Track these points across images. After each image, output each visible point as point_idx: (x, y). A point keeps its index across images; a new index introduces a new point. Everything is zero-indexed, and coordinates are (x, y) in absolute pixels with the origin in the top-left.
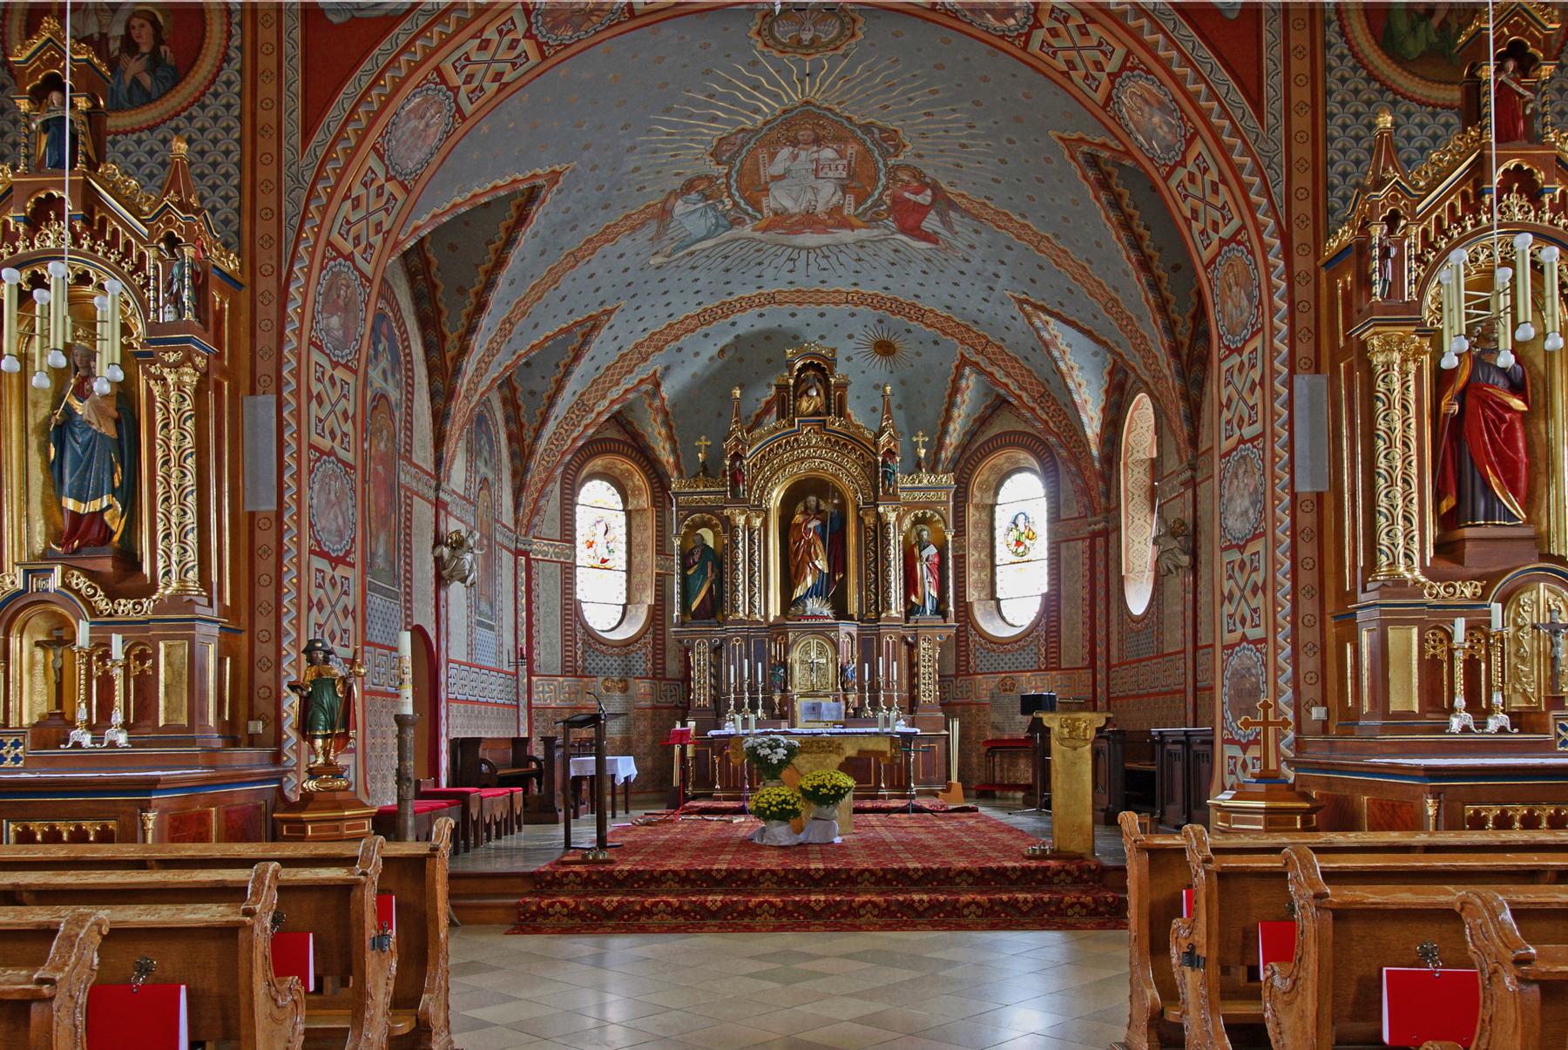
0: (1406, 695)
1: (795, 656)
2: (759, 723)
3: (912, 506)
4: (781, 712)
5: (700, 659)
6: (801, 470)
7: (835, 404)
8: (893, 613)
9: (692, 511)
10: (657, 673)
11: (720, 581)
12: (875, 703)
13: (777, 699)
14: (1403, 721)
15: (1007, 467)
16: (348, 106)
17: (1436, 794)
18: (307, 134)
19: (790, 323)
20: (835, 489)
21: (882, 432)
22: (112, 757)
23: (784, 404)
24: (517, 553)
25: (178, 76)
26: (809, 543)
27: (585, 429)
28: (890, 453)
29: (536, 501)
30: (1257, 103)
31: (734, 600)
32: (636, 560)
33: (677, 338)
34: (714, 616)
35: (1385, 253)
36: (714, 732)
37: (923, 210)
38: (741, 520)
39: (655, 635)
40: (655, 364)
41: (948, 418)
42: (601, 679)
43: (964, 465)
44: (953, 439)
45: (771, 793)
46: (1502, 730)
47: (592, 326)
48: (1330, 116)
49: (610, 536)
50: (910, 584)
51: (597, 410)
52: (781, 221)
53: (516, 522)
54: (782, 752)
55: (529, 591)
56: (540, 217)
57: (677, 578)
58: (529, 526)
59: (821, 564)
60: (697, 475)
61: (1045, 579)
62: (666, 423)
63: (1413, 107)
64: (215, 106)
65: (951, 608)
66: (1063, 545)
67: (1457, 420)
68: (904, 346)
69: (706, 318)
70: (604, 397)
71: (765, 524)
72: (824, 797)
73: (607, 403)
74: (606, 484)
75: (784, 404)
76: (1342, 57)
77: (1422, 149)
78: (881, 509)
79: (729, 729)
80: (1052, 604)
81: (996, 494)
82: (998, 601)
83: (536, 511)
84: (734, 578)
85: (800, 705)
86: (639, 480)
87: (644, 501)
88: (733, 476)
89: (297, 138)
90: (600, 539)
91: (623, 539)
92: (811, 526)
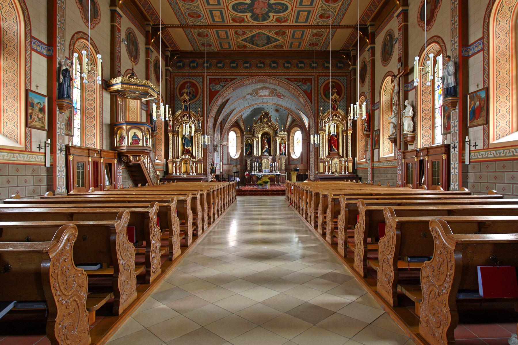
0: (322, 170)
1: (263, 162)
2: (258, 173)
3: (281, 137)
4: (260, 171)
5: (248, 162)
6: (263, 131)
7: (269, 120)
8: (278, 155)
10: (241, 164)
13: (260, 169)
14: (321, 173)
15: (296, 130)
18: (210, 104)
19: (262, 107)
20: (269, 134)
21: (276, 125)
22: (194, 176)
23: (261, 119)
24: (221, 144)
25: (196, 97)
26: (265, 143)
27: (230, 125)
28: (277, 129)
31: (254, 152)
35: (321, 123)
36: (251, 174)
37: (281, 96)
38: (255, 139)
40: (242, 113)
41: (287, 122)
43: (289, 131)
44: (288, 125)
45: (260, 182)
47: (233, 110)
48: (319, 104)
50: (280, 150)
52: (261, 96)
53: (221, 140)
54: (261, 176)
55: (222, 151)
56: (229, 101)
57: (245, 149)
58: (222, 140)
59: (267, 146)
62: (243, 122)
64: (199, 101)
67: (330, 140)
69: (249, 106)
71: (258, 140)
72: (266, 183)
75: (261, 119)
77: (327, 109)
79: (253, 173)
80: (302, 154)
83: (223, 138)
84: (254, 149)
85: (264, 169)
86: (238, 131)
87: (239, 135)
88: (254, 132)
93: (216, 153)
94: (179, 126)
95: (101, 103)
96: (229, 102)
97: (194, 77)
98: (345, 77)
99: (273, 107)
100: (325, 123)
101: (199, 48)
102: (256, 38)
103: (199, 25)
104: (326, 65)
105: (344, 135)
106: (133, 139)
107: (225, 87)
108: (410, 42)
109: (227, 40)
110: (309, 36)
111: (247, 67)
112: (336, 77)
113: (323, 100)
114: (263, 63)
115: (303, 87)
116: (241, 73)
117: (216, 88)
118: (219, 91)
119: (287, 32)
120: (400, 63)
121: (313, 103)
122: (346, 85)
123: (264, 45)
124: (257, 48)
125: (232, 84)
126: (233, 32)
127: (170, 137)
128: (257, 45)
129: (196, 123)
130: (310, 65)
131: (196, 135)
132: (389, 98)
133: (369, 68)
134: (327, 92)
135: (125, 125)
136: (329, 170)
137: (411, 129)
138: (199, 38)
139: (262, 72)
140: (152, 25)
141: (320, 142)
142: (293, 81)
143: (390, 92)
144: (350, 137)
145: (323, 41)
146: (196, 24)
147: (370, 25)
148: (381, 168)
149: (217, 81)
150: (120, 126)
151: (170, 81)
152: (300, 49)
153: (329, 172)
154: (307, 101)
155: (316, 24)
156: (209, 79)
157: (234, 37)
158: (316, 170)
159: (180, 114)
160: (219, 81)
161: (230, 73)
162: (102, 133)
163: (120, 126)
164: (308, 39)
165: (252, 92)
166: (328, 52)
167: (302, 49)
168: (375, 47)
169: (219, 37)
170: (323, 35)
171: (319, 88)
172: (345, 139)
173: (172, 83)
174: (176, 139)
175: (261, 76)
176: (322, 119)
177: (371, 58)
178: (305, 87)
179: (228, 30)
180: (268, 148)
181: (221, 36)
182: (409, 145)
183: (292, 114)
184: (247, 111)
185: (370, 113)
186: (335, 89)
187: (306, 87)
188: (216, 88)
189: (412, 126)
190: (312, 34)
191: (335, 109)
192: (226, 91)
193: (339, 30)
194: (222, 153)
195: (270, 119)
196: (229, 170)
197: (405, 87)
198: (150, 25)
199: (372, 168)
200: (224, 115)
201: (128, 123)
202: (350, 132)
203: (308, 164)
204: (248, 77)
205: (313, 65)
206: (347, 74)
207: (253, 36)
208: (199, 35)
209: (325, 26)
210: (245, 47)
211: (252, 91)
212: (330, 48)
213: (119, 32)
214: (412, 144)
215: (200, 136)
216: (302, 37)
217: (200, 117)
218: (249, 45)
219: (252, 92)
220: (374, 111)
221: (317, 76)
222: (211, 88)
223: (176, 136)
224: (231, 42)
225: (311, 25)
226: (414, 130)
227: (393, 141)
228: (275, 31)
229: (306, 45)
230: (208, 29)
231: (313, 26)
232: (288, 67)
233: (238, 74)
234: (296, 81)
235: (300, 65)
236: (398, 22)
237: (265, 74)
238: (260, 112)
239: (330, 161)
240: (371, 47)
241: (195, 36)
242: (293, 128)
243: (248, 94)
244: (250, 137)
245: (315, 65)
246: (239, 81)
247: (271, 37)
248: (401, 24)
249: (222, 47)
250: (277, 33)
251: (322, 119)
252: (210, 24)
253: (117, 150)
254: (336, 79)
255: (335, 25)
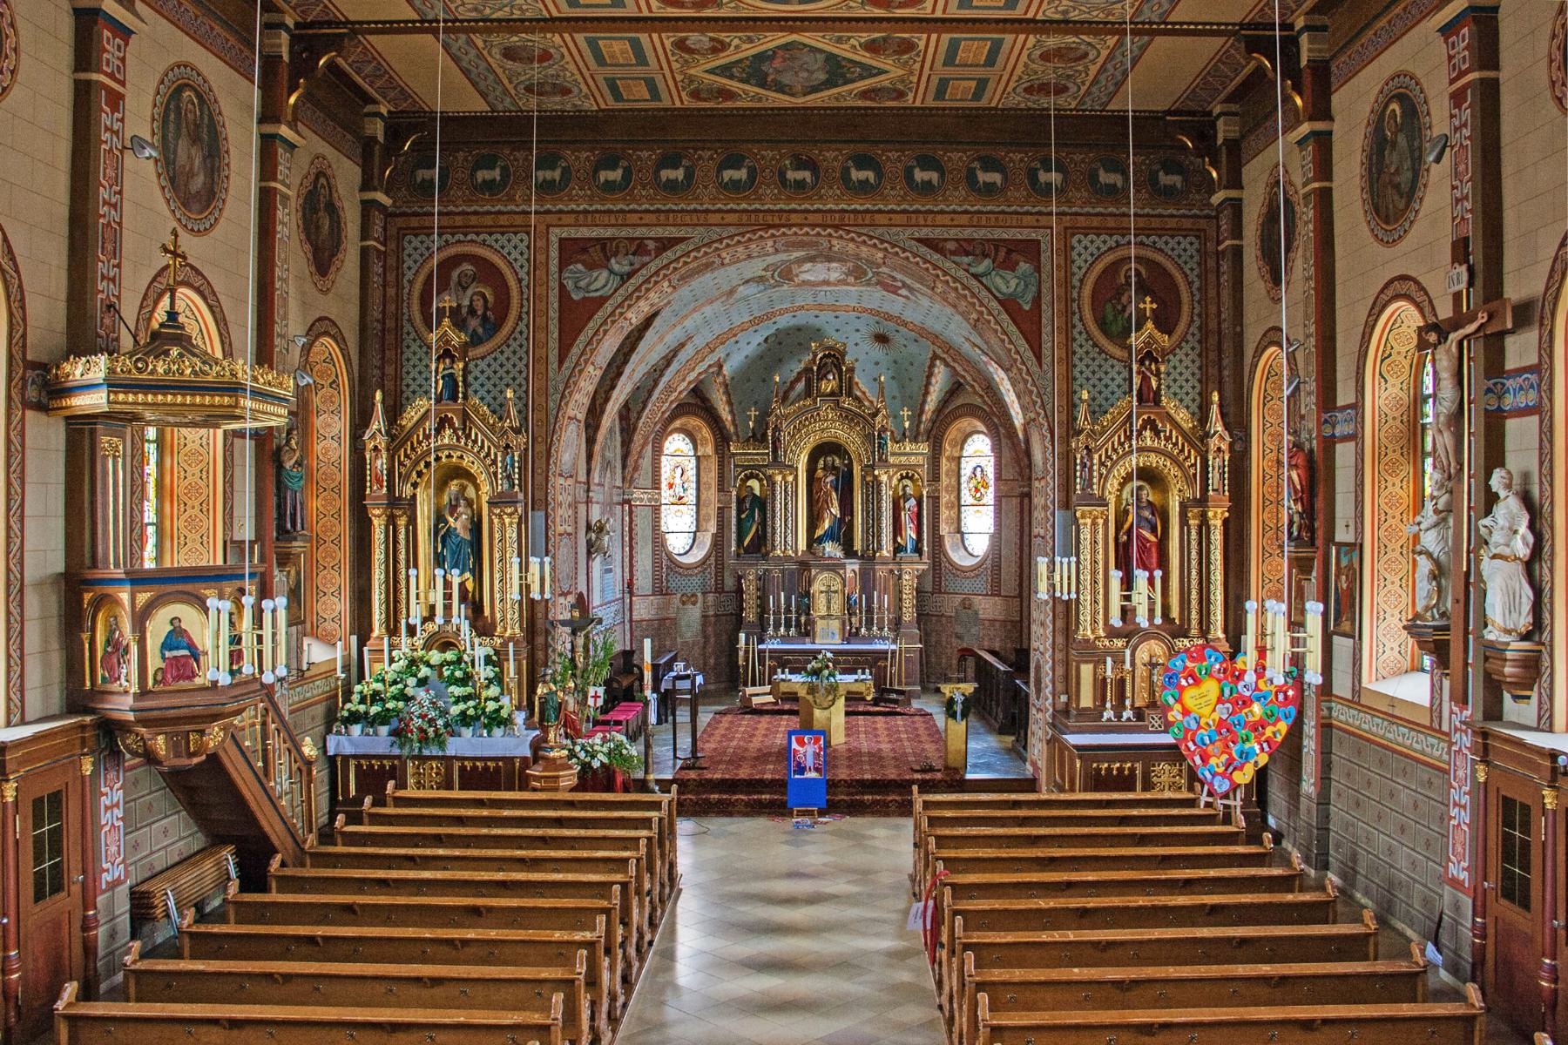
3: (900, 467)
4: (807, 632)
7: (847, 387)
8: (885, 553)
9: (746, 468)
11: (763, 523)
12: (869, 623)
14: (1083, 713)
15: (969, 429)
16: (581, 347)
17: (1080, 757)
18: (561, 362)
19: (813, 321)
20: (846, 452)
23: (811, 377)
28: (884, 429)
29: (636, 461)
30: (1039, 357)
32: (703, 497)
33: (735, 335)
34: (759, 551)
35: (1084, 465)
38: (779, 478)
39: (716, 556)
40: (720, 353)
41: (927, 393)
42: (679, 596)
43: (935, 435)
46: (1129, 719)
49: (685, 477)
50: (897, 528)
51: (679, 389)
52: (804, 283)
56: (657, 322)
59: (835, 510)
60: (748, 440)
61: (992, 521)
62: (727, 393)
63: (1115, 362)
65: (925, 549)
66: (1004, 500)
68: (898, 339)
69: (756, 321)
70: (684, 380)
73: (685, 384)
74: (682, 436)
76: (1080, 333)
78: (876, 472)
80: (996, 538)
81: (962, 449)
82: (962, 534)
83: (636, 469)
86: (706, 433)
87: (709, 450)
88: (774, 443)
89: (556, 365)
90: (678, 481)
91: (694, 479)
92: (828, 480)
93: (597, 564)
94: (420, 474)
95: (16, 484)
96: (655, 324)
97: (490, 234)
98: (1193, 239)
99: (867, 326)
100: (1102, 464)
101: (514, 103)
102: (777, 64)
103: (508, 21)
104: (1105, 178)
105: (1191, 522)
106: (168, 654)
107: (632, 281)
108: (1507, 169)
109: (639, 71)
110: (1024, 58)
111: (735, 186)
112: (1152, 238)
113: (1095, 345)
114: (811, 165)
115: (999, 281)
116: (707, 211)
117: (589, 284)
118: (603, 300)
119: (922, 44)
120: (1463, 270)
121: (1046, 360)
122: (1199, 276)
123: (815, 89)
124: (784, 100)
125: (666, 266)
126: (668, 43)
127: (377, 531)
128: (781, 88)
129: (494, 462)
130: (1032, 175)
131: (496, 521)
132: (1401, 394)
133: (1306, 229)
134: (1109, 307)
135: (128, 587)
136: (1121, 696)
137: (1524, 621)
138: (509, 64)
139: (808, 207)
140: (292, 26)
141: (1078, 592)
142: (953, 253)
143: (1406, 363)
144: (1217, 537)
145: (1091, 78)
146: (494, 16)
147: (1307, 28)
148: (1368, 740)
149: (595, 253)
150: (109, 590)
151: (383, 255)
152: (983, 103)
153: (1119, 707)
154: (1017, 352)
155: (1058, 17)
156: (561, 240)
157: (671, 58)
158: (1060, 687)
159: (425, 417)
160: (607, 249)
161: (658, 211)
162: (22, 633)
163: (109, 590)
164: (1020, 68)
165: (764, 273)
166: (1119, 117)
167: (993, 105)
168: (1330, 133)
169: (600, 59)
170: (1091, 57)
171: (1073, 287)
172: (1194, 544)
173: (391, 261)
174: (402, 536)
175: (801, 226)
176: (1087, 447)
177: (1316, 185)
178: (1006, 283)
179: (643, 38)
180: (841, 520)
181: (613, 56)
182: (1507, 697)
183: (949, 360)
184: (742, 344)
185: (1311, 451)
186: (1148, 299)
187: (1013, 283)
188: (592, 287)
189: (1526, 606)
190: (1038, 53)
191: (1148, 397)
192: (639, 298)
193: (1159, 40)
194: (631, 539)
195: (851, 379)
196: (662, 620)
197: (1489, 391)
198: (282, 25)
199: (1323, 725)
200: (637, 376)
201: (138, 579)
202: (1219, 511)
203: (1020, 595)
204: (742, 234)
205: (1043, 177)
206: (1203, 223)
207: (761, 58)
208: (509, 53)
209: (1098, 23)
210: (728, 94)
211: (764, 270)
212: (1128, 102)
213: (115, 109)
214: (1527, 693)
215: (511, 524)
216: (991, 61)
217: (511, 434)
218: (747, 87)
219: (764, 273)
220: (1335, 443)
221: (1066, 228)
222: (569, 284)
223: (402, 522)
224: (659, 80)
225: (1033, 21)
226: (1538, 626)
227: (1432, 645)
228: (863, 40)
229: (1009, 89)
230: (549, 35)
231: (1044, 22)
232: (927, 188)
233: (694, 216)
234: (967, 254)
235: (983, 177)
236: (1450, 58)
237: (818, 218)
238: (803, 347)
239: (1128, 652)
240: (1314, 134)
241: (495, 59)
242: (956, 418)
243: (747, 282)
244: (758, 467)
245: (1054, 177)
246: (697, 249)
247: (844, 58)
248: (1462, 74)
249: (617, 96)
250: (871, 47)
251: (1087, 447)
252: (555, 14)
253: (92, 711)
254: (1153, 246)
255: (1143, 23)
